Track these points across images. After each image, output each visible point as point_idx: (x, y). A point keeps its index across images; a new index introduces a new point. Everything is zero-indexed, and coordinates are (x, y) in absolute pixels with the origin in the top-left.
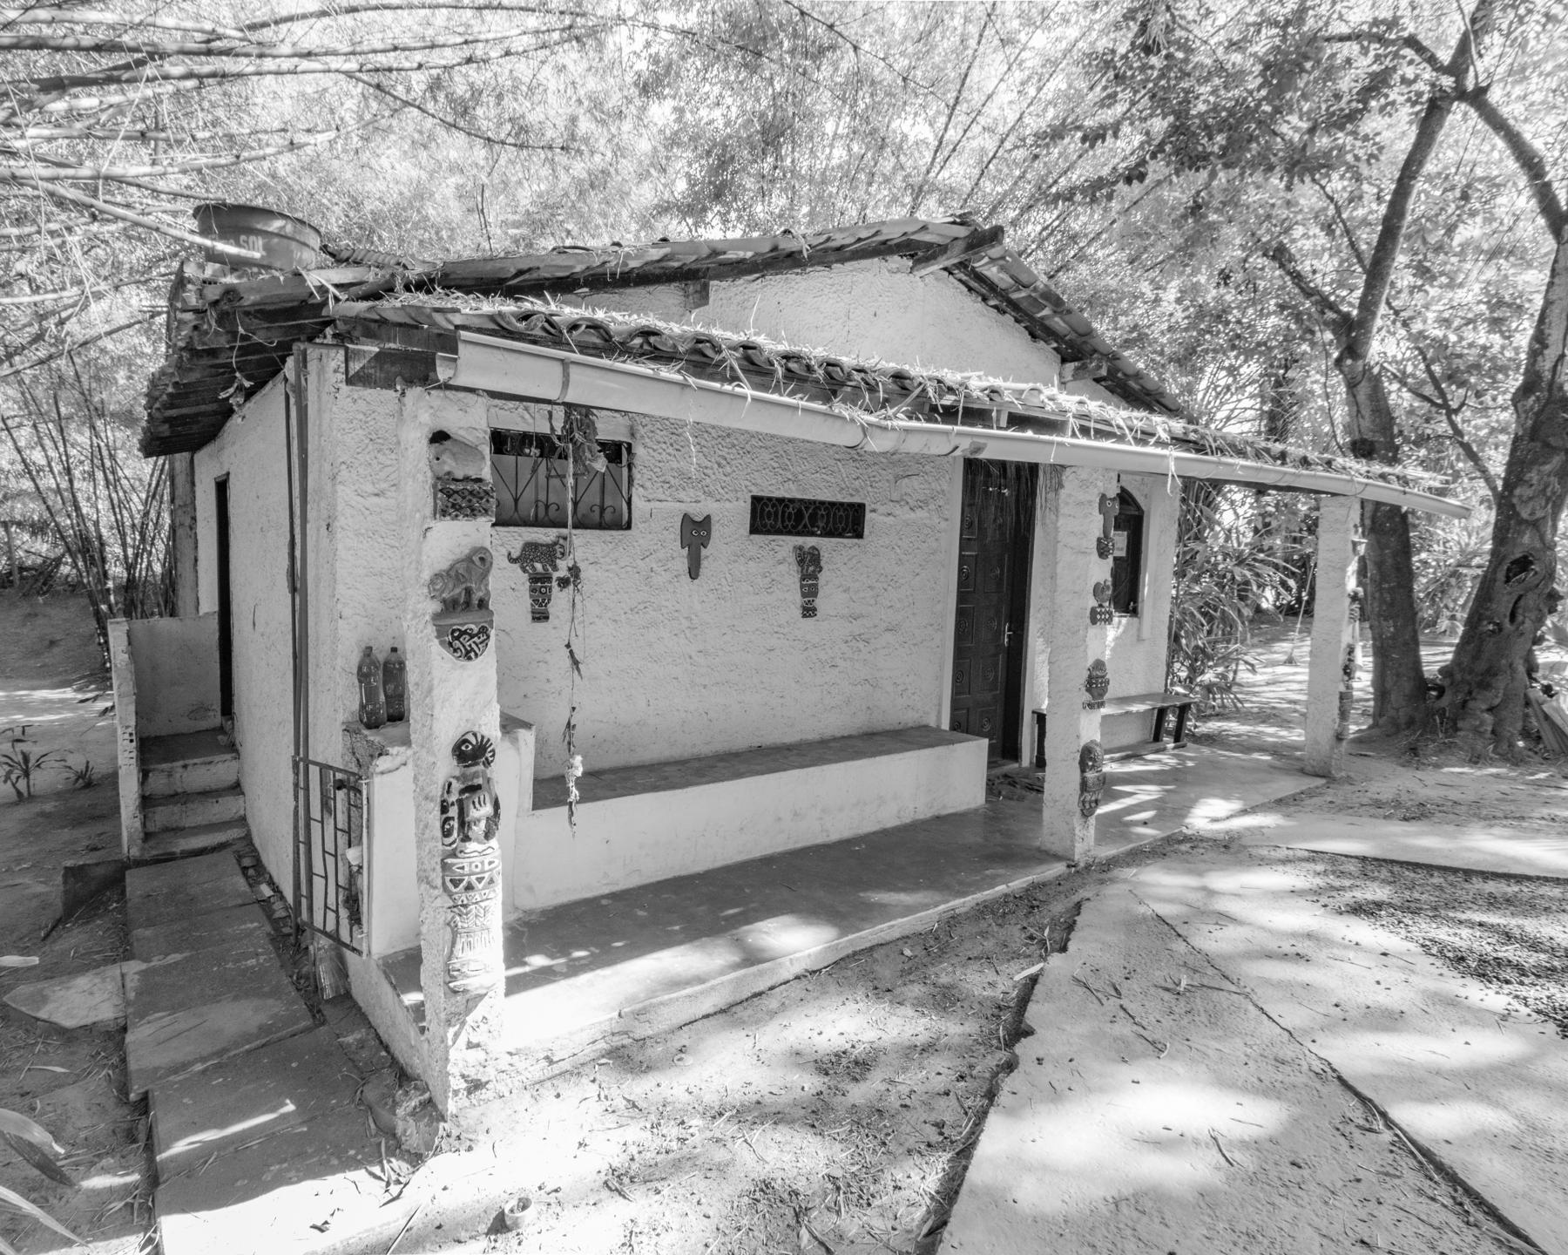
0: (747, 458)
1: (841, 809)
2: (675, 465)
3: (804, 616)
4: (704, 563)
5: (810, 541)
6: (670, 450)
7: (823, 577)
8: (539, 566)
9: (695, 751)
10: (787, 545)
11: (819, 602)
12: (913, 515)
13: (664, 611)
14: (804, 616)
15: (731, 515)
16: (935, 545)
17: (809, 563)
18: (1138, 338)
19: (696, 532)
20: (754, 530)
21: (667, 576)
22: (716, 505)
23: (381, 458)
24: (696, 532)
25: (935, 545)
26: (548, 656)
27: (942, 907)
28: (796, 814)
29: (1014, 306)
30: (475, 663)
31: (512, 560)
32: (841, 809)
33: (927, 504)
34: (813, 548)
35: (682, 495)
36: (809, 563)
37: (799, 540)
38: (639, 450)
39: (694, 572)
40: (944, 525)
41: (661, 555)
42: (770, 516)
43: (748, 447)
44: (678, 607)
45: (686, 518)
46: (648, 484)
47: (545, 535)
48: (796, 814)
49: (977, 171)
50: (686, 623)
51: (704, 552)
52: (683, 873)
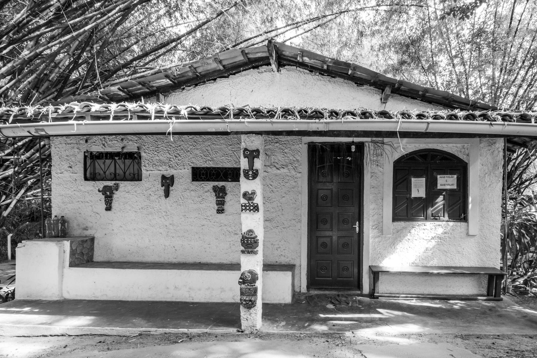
0: (189, 154)
1: (200, 290)
2: (158, 158)
3: (217, 213)
4: (171, 192)
5: (221, 184)
6: (155, 153)
7: (228, 198)
8: (108, 193)
9: (170, 260)
10: (209, 185)
11: (226, 207)
12: (278, 171)
13: (155, 209)
14: (217, 213)
15: (183, 175)
16: (294, 184)
17: (220, 193)
18: (489, 67)
19: (168, 182)
20: (193, 180)
21: (156, 197)
22: (175, 171)
23: (62, 163)
24: (168, 182)
25: (294, 184)
26: (112, 222)
27: (144, 329)
28: (176, 287)
29: (325, 71)
30: (248, 229)
31: (99, 191)
32: (200, 290)
33: (287, 166)
34: (223, 186)
35: (160, 168)
36: (220, 193)
37: (216, 183)
38: (143, 154)
39: (167, 194)
40: (299, 175)
41: (153, 189)
42: (199, 174)
43: (189, 149)
44: (161, 208)
45: (164, 177)
46: (147, 165)
47: (110, 183)
48: (176, 287)
49: (342, 14)
50: (164, 214)
51: (171, 188)
52: (124, 300)
